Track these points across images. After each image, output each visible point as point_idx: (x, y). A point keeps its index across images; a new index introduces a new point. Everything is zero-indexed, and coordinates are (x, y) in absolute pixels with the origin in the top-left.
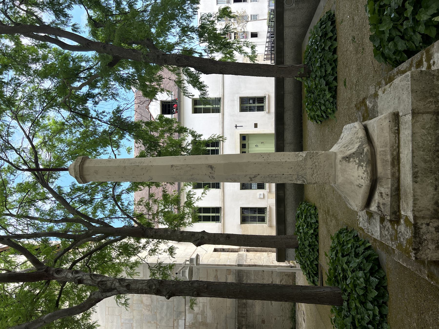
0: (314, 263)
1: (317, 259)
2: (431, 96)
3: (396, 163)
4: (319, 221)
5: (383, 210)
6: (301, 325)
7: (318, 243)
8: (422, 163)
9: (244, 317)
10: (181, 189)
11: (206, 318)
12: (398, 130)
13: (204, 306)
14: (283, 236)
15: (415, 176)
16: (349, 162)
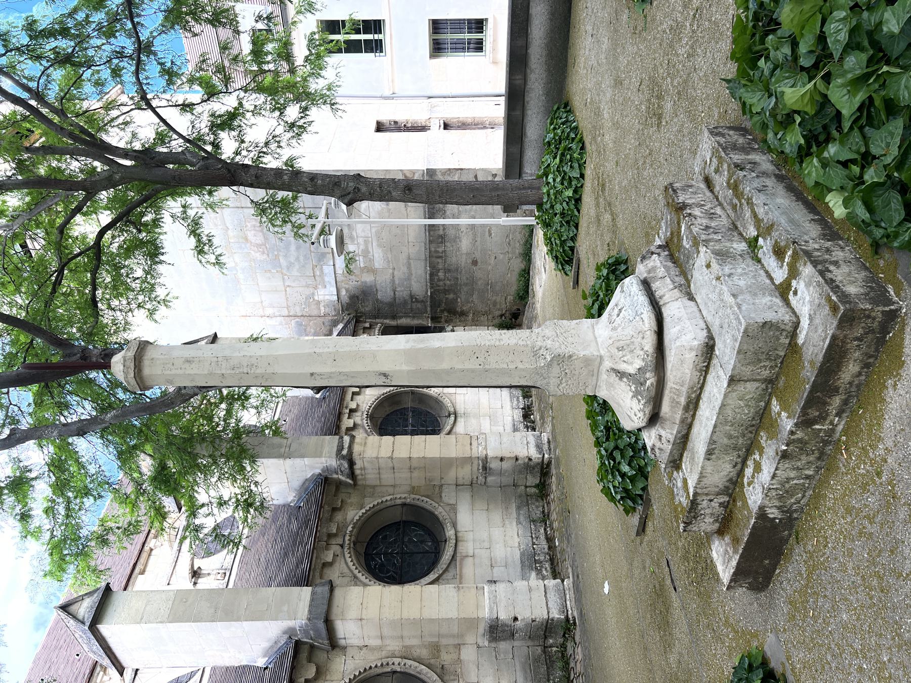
0: (568, 245)
1: (573, 239)
2: (769, 359)
3: (691, 407)
4: (586, 176)
5: (658, 455)
6: (540, 273)
7: (579, 213)
8: (725, 439)
9: (441, 257)
10: (290, 21)
11: (372, 261)
12: (708, 367)
13: (366, 242)
14: (515, 182)
15: (709, 453)
16: (621, 379)
